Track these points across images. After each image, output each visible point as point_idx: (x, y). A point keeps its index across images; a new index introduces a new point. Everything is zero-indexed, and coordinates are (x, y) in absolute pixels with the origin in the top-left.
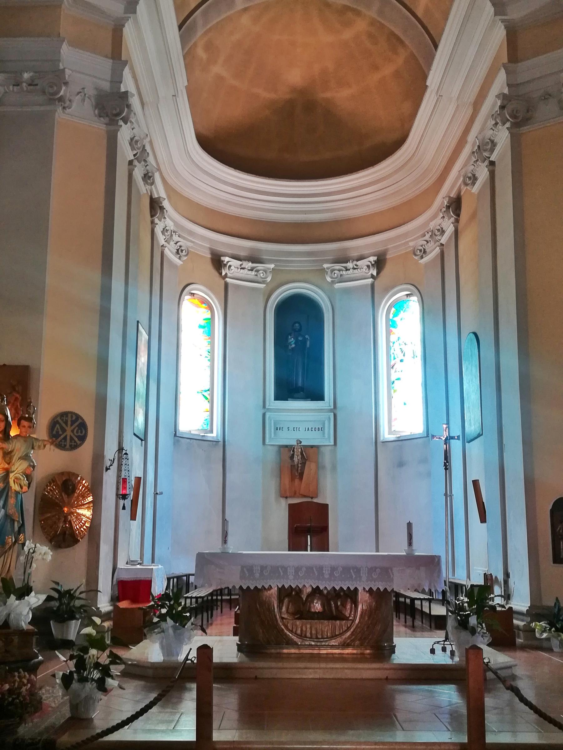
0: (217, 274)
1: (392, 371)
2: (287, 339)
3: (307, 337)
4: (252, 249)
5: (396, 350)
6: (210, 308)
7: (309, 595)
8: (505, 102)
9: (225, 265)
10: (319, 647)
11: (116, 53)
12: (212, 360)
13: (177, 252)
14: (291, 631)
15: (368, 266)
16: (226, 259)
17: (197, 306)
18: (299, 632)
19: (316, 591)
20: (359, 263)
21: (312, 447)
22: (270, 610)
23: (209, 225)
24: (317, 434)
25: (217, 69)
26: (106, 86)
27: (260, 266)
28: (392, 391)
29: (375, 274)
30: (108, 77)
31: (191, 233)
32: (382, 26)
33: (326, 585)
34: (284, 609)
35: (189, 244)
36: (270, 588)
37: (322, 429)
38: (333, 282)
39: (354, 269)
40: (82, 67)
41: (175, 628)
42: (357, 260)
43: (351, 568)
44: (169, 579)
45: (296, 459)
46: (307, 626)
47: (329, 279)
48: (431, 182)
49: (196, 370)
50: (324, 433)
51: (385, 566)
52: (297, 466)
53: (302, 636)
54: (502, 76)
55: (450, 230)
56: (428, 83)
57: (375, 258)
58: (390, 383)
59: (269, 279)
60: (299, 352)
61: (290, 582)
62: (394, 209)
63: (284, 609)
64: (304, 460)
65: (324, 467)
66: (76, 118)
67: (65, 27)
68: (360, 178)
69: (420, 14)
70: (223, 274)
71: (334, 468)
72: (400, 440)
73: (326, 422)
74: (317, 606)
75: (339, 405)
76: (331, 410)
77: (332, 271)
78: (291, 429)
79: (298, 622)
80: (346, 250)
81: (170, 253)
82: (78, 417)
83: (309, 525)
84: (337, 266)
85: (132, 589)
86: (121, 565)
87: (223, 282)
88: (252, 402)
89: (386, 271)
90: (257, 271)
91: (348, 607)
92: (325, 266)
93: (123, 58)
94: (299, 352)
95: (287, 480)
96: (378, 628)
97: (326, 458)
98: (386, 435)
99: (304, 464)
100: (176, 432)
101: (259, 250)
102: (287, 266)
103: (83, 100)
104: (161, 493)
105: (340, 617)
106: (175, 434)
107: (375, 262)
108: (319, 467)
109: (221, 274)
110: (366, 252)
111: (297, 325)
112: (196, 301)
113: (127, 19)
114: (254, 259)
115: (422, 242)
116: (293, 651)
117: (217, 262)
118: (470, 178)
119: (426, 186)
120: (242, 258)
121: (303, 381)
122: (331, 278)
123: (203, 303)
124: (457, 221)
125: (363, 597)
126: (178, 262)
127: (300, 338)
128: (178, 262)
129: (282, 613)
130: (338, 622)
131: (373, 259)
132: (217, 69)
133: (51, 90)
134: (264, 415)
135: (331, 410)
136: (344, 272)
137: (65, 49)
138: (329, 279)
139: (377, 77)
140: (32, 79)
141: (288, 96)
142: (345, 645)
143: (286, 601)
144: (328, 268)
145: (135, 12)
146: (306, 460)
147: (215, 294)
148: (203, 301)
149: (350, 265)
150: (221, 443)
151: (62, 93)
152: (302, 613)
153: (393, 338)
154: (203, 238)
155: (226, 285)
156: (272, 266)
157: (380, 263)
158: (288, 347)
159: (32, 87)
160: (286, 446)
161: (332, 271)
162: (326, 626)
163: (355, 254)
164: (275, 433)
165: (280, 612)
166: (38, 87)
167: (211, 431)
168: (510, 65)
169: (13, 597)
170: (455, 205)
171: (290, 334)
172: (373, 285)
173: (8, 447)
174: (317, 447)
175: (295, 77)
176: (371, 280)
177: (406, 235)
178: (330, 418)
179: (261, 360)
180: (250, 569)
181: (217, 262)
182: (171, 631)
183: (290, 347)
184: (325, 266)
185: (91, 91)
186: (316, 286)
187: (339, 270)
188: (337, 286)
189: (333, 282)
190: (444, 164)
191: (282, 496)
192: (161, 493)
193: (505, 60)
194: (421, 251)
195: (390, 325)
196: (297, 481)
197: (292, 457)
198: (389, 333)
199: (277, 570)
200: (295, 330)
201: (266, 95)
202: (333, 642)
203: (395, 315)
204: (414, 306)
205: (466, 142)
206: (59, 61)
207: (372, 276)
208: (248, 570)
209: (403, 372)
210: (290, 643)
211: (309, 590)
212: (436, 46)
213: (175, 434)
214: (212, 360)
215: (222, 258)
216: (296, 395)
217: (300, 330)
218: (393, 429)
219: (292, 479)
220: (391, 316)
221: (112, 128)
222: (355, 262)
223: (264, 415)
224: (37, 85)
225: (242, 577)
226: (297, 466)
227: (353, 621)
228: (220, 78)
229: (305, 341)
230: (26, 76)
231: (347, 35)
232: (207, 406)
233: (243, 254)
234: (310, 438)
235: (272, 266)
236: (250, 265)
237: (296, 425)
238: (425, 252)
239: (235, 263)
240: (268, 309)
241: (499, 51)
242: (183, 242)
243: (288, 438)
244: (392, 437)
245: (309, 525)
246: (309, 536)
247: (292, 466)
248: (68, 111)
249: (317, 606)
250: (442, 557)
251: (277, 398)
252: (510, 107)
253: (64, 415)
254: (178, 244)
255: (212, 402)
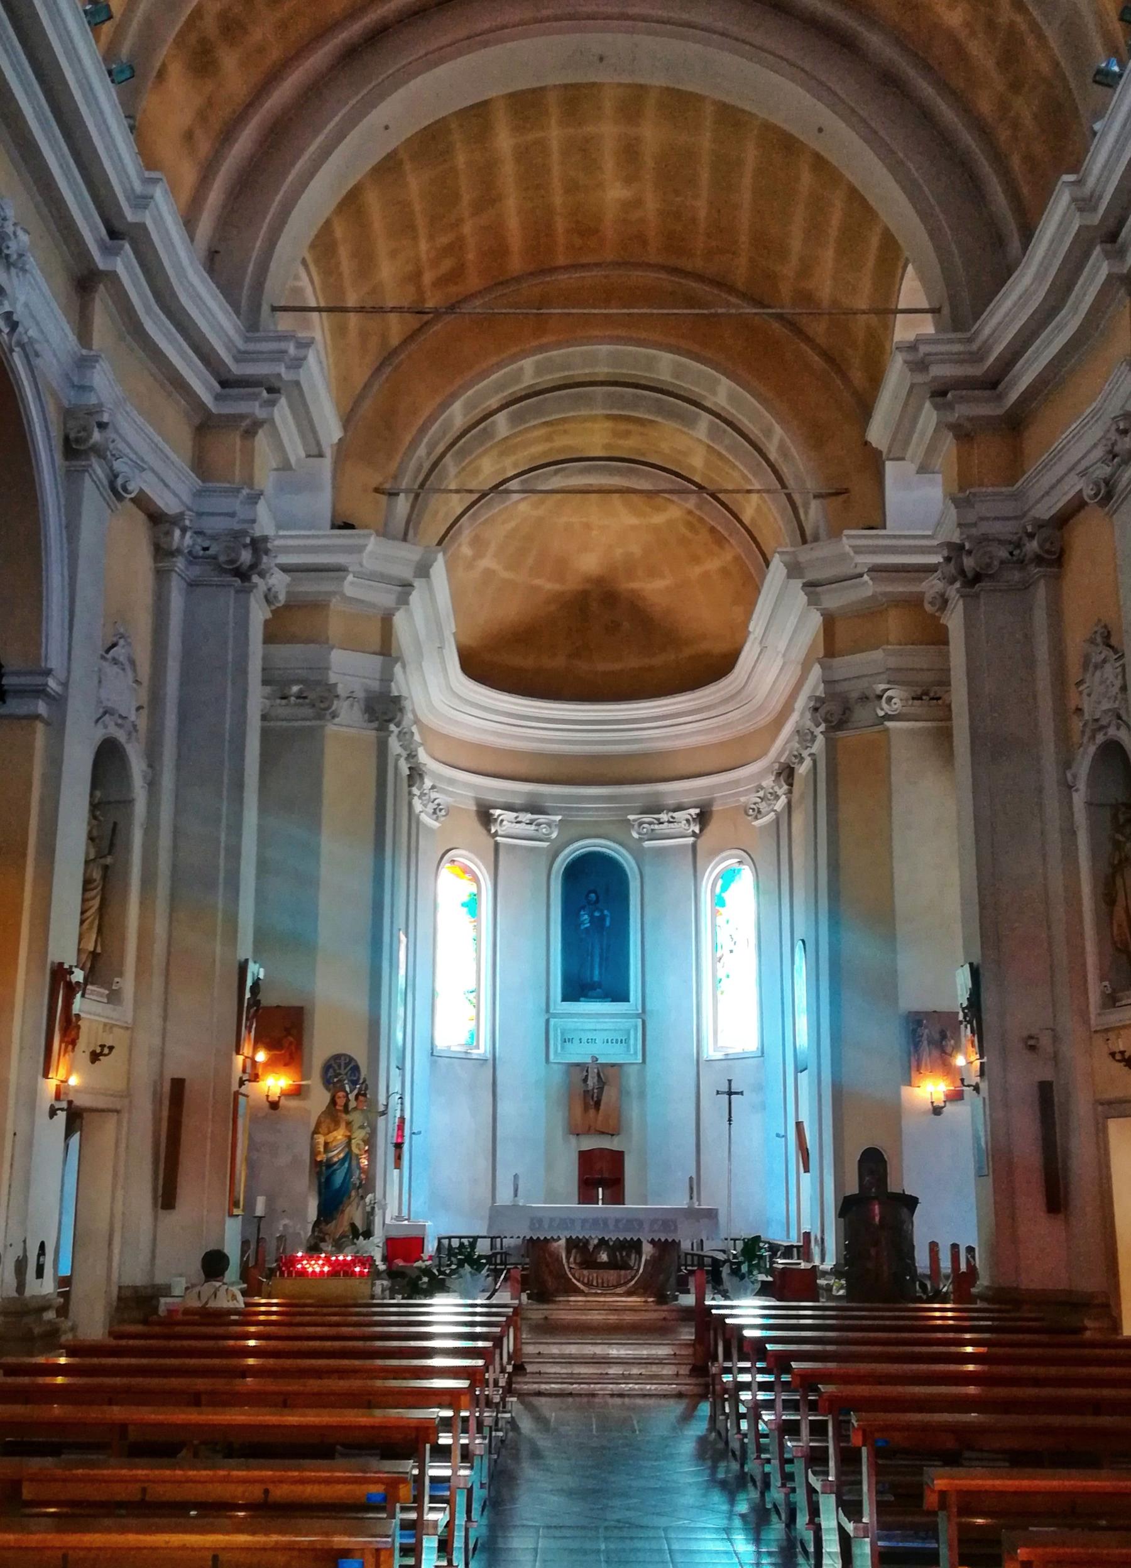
0: (485, 832)
1: (719, 965)
2: (578, 915)
3: (606, 912)
4: (530, 794)
5: (723, 938)
6: (475, 879)
7: (596, 1247)
8: (818, 705)
9: (496, 820)
10: (604, 1295)
11: (386, 648)
12: (478, 950)
13: (435, 813)
14: (578, 1280)
15: (688, 821)
16: (497, 812)
17: (458, 876)
18: (586, 1281)
19: (603, 1242)
20: (675, 815)
21: (613, 1065)
22: (558, 1260)
23: (473, 766)
24: (619, 1048)
25: (487, 562)
26: (375, 685)
27: (542, 818)
28: (719, 993)
29: (697, 831)
30: (378, 676)
31: (452, 781)
32: (701, 520)
33: (612, 1236)
34: (572, 1259)
35: (450, 800)
36: (559, 1239)
37: (627, 1041)
38: (641, 840)
39: (669, 822)
40: (350, 670)
41: (472, 1275)
42: (675, 811)
43: (634, 1222)
44: (440, 1239)
45: (590, 1082)
46: (593, 1275)
47: (635, 835)
48: (769, 719)
49: (461, 967)
50: (628, 1047)
51: (668, 1220)
52: (593, 1097)
53: (589, 1284)
54: (816, 671)
55: (783, 800)
56: (751, 629)
57: (698, 811)
58: (716, 982)
59: (554, 835)
60: (595, 922)
61: (577, 1233)
62: (722, 744)
63: (572, 1259)
64: (602, 1083)
65: (628, 1093)
66: (346, 725)
67: (335, 627)
68: (680, 703)
69: (746, 520)
70: (493, 831)
71: (642, 1095)
72: (727, 1058)
73: (632, 1032)
74: (604, 1257)
75: (648, 1007)
76: (638, 1016)
77: (641, 824)
78: (584, 1040)
79: (585, 1272)
80: (657, 794)
81: (425, 819)
82: (351, 1059)
83: (601, 1174)
84: (647, 818)
85: (405, 1247)
86: (388, 1221)
87: (492, 842)
88: (533, 1003)
89: (713, 827)
90: (539, 825)
91: (633, 1256)
92: (631, 817)
93: (394, 655)
94: (595, 922)
95: (578, 1110)
96: (661, 1277)
97: (632, 1081)
98: (710, 1052)
99: (601, 1089)
100: (432, 1049)
101: (541, 795)
102: (577, 816)
103: (352, 705)
104: (419, 1133)
105: (625, 1266)
106: (432, 1054)
107: (697, 815)
108: (622, 1092)
109: (489, 830)
110: (685, 800)
111: (593, 895)
112: (458, 870)
113: (398, 609)
114: (534, 807)
115: (754, 798)
116: (580, 1299)
117: (485, 816)
118: (795, 756)
119: (762, 723)
120: (517, 807)
121: (600, 974)
122: (639, 834)
123: (465, 872)
124: (790, 792)
125: (648, 1250)
126: (435, 824)
127: (597, 914)
128: (435, 824)
129: (568, 1263)
130: (623, 1272)
131: (694, 811)
132: (487, 562)
133: (322, 705)
134: (547, 1022)
135: (638, 1016)
136: (656, 827)
137: (338, 657)
138: (635, 835)
139: (697, 570)
140: (301, 691)
141: (580, 587)
142: (629, 1293)
143: (574, 1251)
144: (634, 820)
145: (406, 603)
146: (604, 1084)
147: (481, 858)
148: (466, 870)
149: (664, 817)
150: (491, 1062)
151: (334, 708)
152: (588, 1262)
153: (720, 920)
154: (466, 785)
155: (497, 844)
156: (559, 818)
157: (704, 817)
158: (580, 925)
159: (301, 701)
160: (578, 1065)
161: (641, 824)
162: (611, 1275)
163: (671, 802)
164: (563, 1048)
165: (568, 1262)
166: (307, 701)
167: (478, 1047)
168: (825, 659)
169: (361, 1238)
170: (787, 773)
171: (583, 908)
172: (694, 846)
173: (350, 1117)
174: (619, 1066)
175: (589, 563)
176: (692, 839)
177: (736, 783)
178: (636, 1026)
179: (541, 947)
180: (540, 1221)
181: (485, 816)
182: (469, 1275)
183: (582, 927)
184: (631, 817)
185: (361, 695)
186: (621, 844)
187: (650, 823)
188: (647, 844)
189: (641, 840)
190: (789, 690)
191: (571, 1133)
192: (419, 1133)
193: (821, 655)
194: (753, 810)
195: (719, 902)
196: (592, 1112)
197: (585, 1080)
198: (715, 914)
199: (566, 1222)
200: (589, 903)
201: (551, 586)
202: (619, 1290)
203: (724, 888)
204: (747, 875)
205: (793, 710)
206: (328, 668)
207: (694, 834)
208: (536, 1221)
209: (732, 975)
210: (577, 1291)
211: (596, 1241)
212: (768, 566)
213: (432, 1054)
214: (478, 950)
215: (492, 811)
216: (594, 993)
217: (597, 901)
218: (719, 1044)
219: (586, 1108)
220: (718, 889)
221: (382, 734)
222: (671, 814)
223: (547, 1022)
224: (305, 698)
225: (531, 1228)
226: (593, 1097)
227: (638, 1271)
228: (489, 573)
229: (602, 918)
230: (295, 689)
231: (659, 519)
232: (473, 1012)
233: (518, 801)
234: (610, 1054)
235: (559, 818)
236: (529, 816)
237: (590, 1036)
238: (759, 812)
239: (510, 815)
240: (553, 876)
241: (814, 641)
242: (442, 799)
243: (579, 1054)
244: (719, 1055)
245: (601, 1174)
246: (600, 1190)
247: (586, 1092)
248: (337, 720)
249: (604, 1257)
250: (720, 1212)
251: (565, 999)
252: (822, 711)
253: (337, 1057)
254: (436, 802)
255: (478, 1007)
